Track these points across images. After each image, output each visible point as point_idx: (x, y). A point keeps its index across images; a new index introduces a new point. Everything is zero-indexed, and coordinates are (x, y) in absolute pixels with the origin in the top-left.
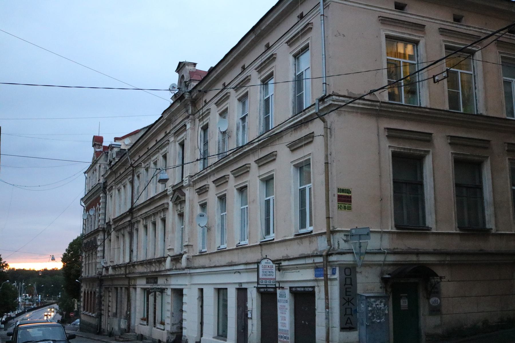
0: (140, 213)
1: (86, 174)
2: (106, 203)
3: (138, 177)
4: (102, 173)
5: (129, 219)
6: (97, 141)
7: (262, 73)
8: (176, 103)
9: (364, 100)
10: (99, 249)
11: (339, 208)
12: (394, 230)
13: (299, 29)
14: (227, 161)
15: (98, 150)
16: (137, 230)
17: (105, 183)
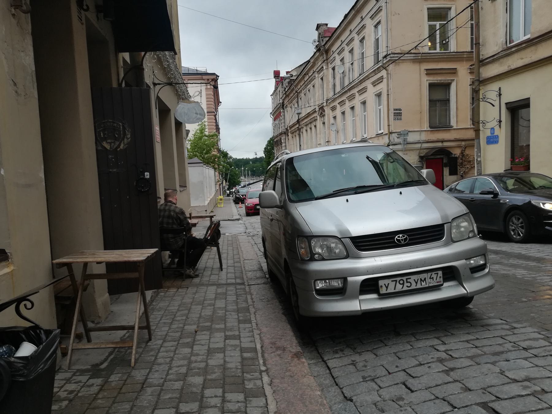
0: (303, 123)
1: (272, 96)
2: (284, 115)
3: (301, 99)
4: (281, 96)
5: (297, 126)
6: (277, 74)
7: (360, 36)
8: (317, 53)
9: (411, 53)
10: (283, 145)
11: (395, 119)
12: (429, 129)
13: (374, 12)
14: (344, 91)
15: (277, 80)
16: (302, 132)
17: (283, 103)
